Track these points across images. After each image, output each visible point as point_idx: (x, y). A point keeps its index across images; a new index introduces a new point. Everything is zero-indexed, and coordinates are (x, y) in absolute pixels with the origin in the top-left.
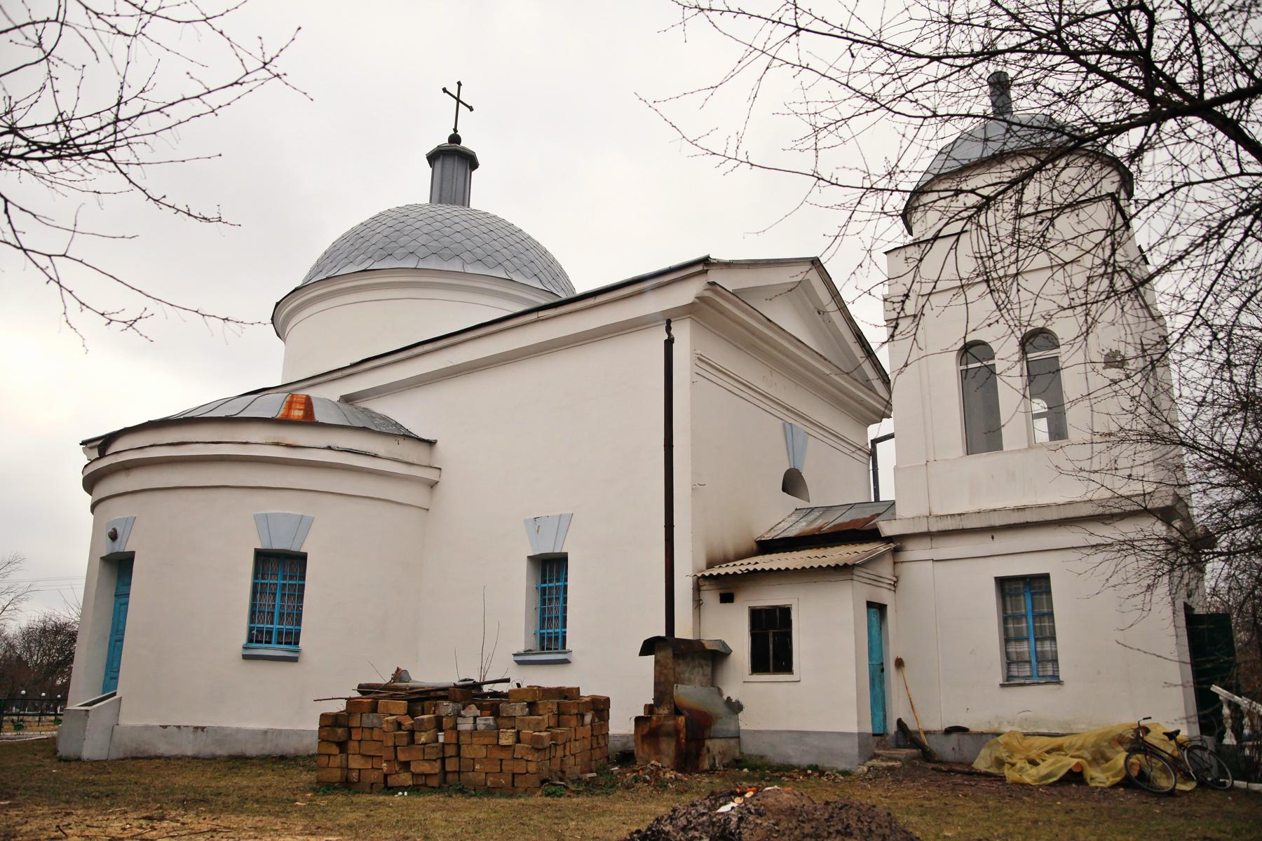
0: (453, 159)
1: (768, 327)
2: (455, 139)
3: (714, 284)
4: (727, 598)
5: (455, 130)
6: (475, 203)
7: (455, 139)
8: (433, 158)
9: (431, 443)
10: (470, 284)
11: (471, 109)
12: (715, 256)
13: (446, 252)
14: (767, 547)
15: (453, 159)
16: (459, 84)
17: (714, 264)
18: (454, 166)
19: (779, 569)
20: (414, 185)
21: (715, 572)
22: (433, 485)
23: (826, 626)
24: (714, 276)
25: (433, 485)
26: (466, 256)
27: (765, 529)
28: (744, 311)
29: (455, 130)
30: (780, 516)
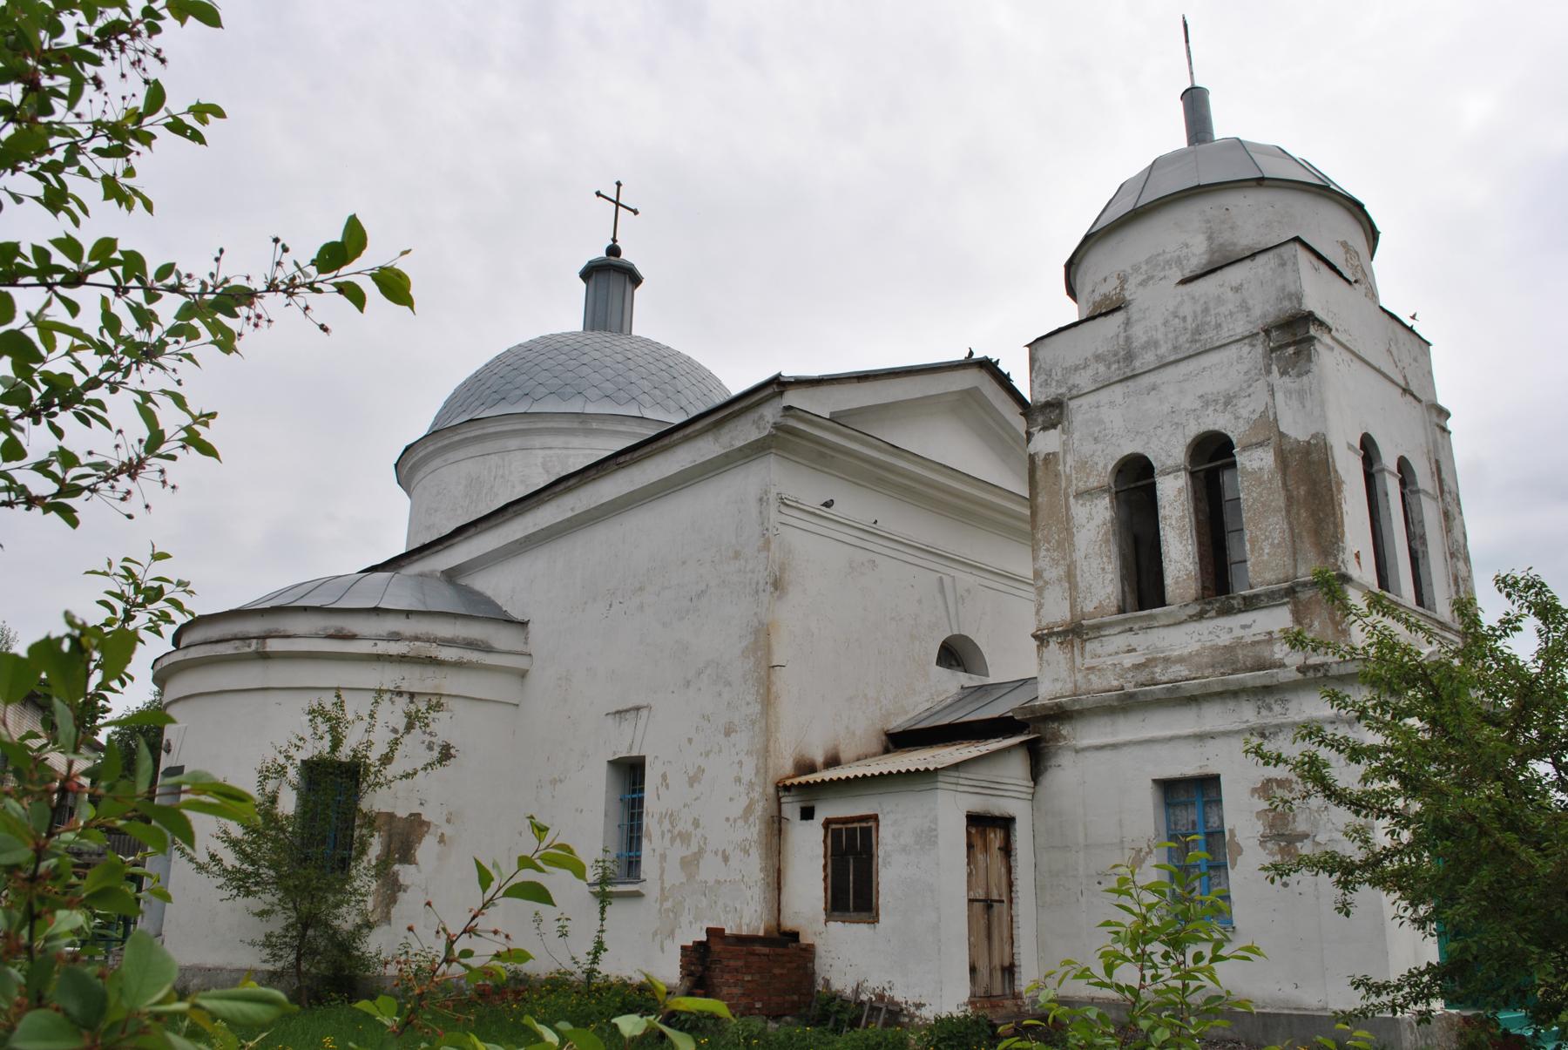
0: (611, 276)
1: (892, 454)
2: (614, 251)
3: (789, 408)
4: (807, 814)
5: (614, 240)
6: (639, 329)
7: (614, 251)
8: (589, 273)
9: (523, 624)
10: (540, 425)
11: (636, 212)
12: (789, 372)
13: (569, 389)
14: (900, 740)
15: (611, 276)
16: (619, 184)
17: (790, 383)
18: (616, 281)
19: (927, 770)
20: (564, 311)
21: (803, 779)
22: (523, 674)
23: (922, 849)
24: (792, 398)
25: (523, 674)
26: (590, 393)
27: (911, 711)
28: (855, 439)
29: (614, 240)
30: (935, 693)
